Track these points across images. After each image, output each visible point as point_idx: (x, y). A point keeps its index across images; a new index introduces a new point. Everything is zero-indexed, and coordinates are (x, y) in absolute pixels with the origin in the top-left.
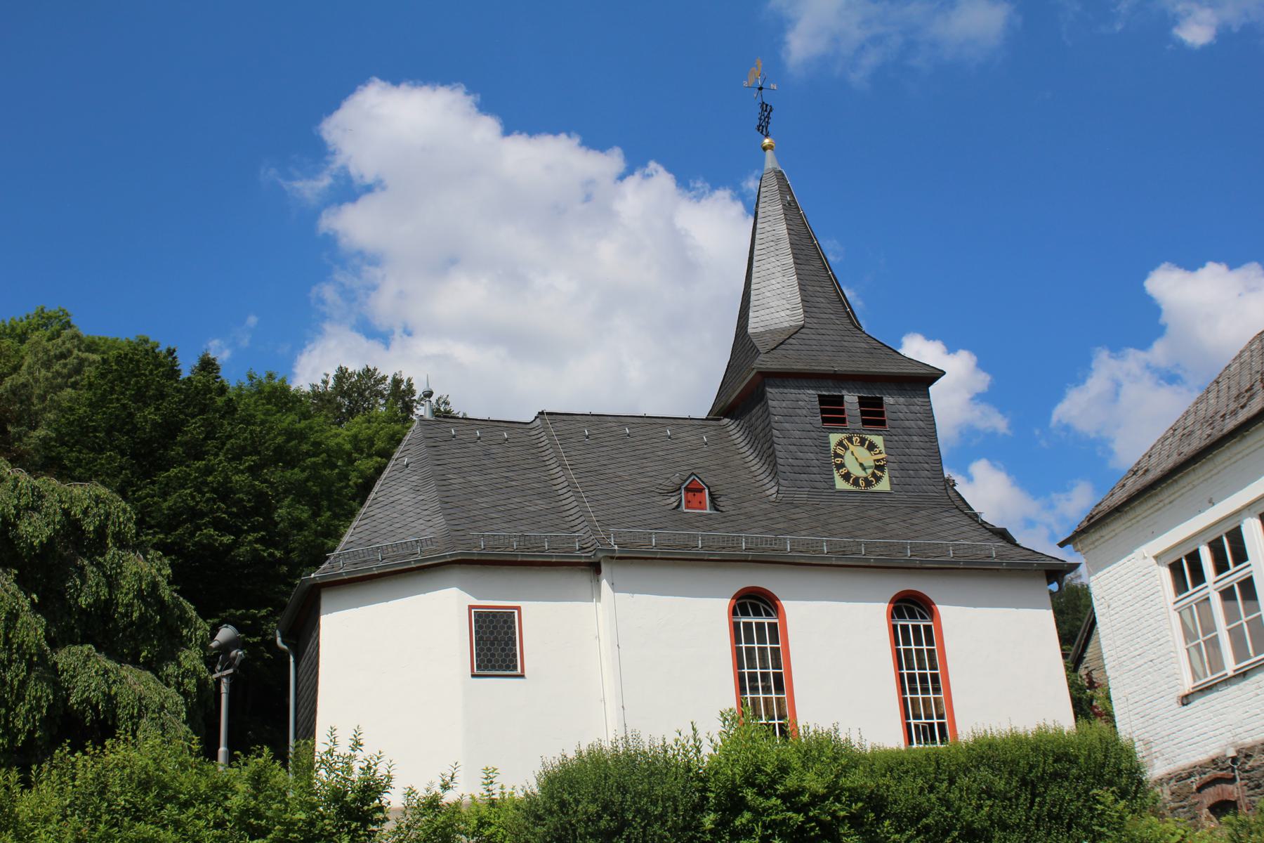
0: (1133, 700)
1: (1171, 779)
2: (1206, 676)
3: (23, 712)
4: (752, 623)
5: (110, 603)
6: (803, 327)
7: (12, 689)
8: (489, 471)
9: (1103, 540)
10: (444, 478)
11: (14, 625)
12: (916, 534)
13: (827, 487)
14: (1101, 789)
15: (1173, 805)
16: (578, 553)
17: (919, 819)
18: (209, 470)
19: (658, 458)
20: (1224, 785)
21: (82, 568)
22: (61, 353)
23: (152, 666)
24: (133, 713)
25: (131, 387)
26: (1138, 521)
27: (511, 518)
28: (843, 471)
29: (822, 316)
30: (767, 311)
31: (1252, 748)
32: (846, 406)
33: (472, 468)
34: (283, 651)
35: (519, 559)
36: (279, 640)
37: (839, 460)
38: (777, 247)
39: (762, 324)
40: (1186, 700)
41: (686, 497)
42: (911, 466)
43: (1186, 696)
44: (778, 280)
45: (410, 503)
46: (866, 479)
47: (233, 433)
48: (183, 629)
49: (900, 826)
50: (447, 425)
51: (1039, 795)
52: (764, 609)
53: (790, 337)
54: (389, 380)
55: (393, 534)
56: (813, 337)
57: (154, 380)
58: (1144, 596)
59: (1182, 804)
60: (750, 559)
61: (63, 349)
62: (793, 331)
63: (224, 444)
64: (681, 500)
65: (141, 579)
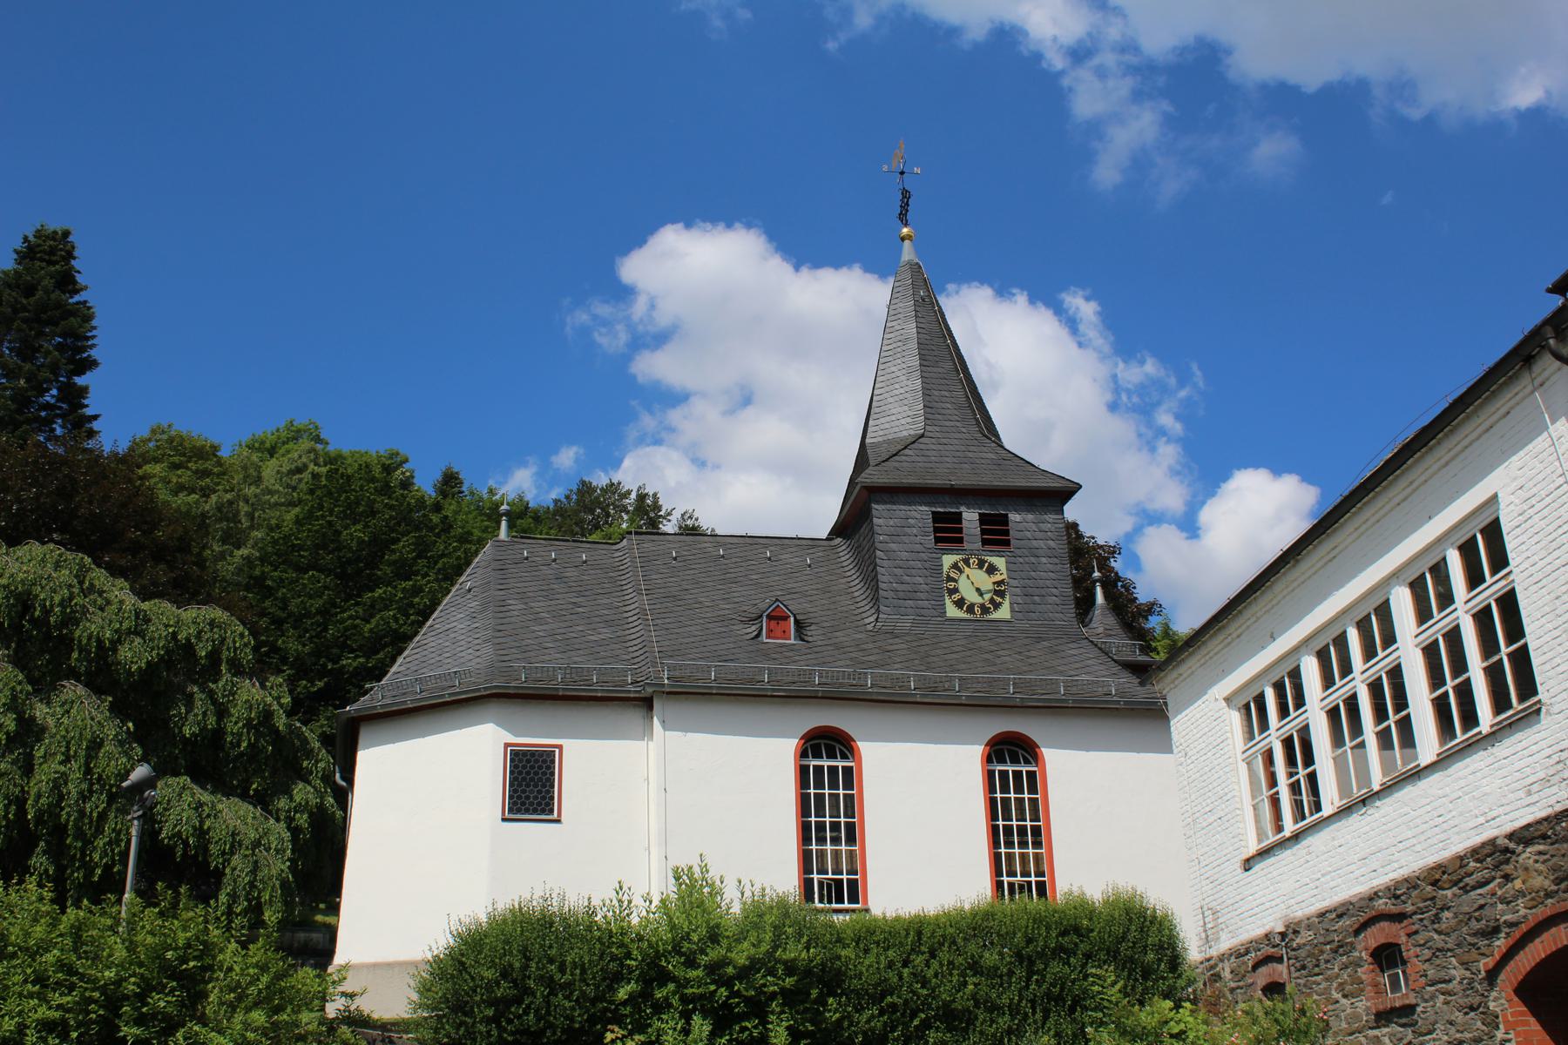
0: (1204, 863)
1: (1231, 955)
2: (1268, 838)
3: (101, 844)
4: (823, 766)
5: (219, 733)
6: (922, 436)
7: (91, 821)
8: (556, 597)
9: (1181, 678)
10: (502, 604)
11: (97, 754)
12: (1031, 668)
13: (937, 614)
14: (1101, 968)
15: (1233, 985)
16: (630, 688)
17: (883, 996)
18: (417, 591)
19: (750, 582)
20: (1275, 964)
21: (192, 695)
22: (297, 467)
23: (262, 801)
24: (224, 849)
25: (340, 503)
26: (1211, 658)
27: (568, 648)
28: (956, 597)
29: (947, 423)
30: (888, 419)
31: (1300, 922)
32: (965, 524)
33: (539, 593)
34: (342, 787)
35: (561, 693)
36: (338, 775)
37: (952, 585)
38: (904, 348)
39: (881, 433)
40: (1248, 864)
41: (768, 625)
42: (1037, 591)
43: (1248, 860)
44: (903, 384)
45: (464, 631)
46: (982, 606)
47: (446, 552)
48: (303, 760)
49: (860, 1004)
50: (522, 546)
51: (1037, 973)
52: (841, 751)
53: (905, 448)
54: (633, 496)
55: (440, 664)
56: (933, 447)
57: (364, 495)
58: (1215, 743)
59: (1241, 984)
60: (820, 695)
61: (299, 464)
62: (909, 441)
63: (436, 563)
64: (762, 629)
65: (251, 708)
